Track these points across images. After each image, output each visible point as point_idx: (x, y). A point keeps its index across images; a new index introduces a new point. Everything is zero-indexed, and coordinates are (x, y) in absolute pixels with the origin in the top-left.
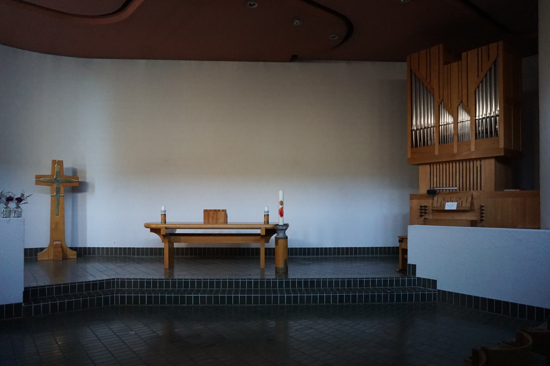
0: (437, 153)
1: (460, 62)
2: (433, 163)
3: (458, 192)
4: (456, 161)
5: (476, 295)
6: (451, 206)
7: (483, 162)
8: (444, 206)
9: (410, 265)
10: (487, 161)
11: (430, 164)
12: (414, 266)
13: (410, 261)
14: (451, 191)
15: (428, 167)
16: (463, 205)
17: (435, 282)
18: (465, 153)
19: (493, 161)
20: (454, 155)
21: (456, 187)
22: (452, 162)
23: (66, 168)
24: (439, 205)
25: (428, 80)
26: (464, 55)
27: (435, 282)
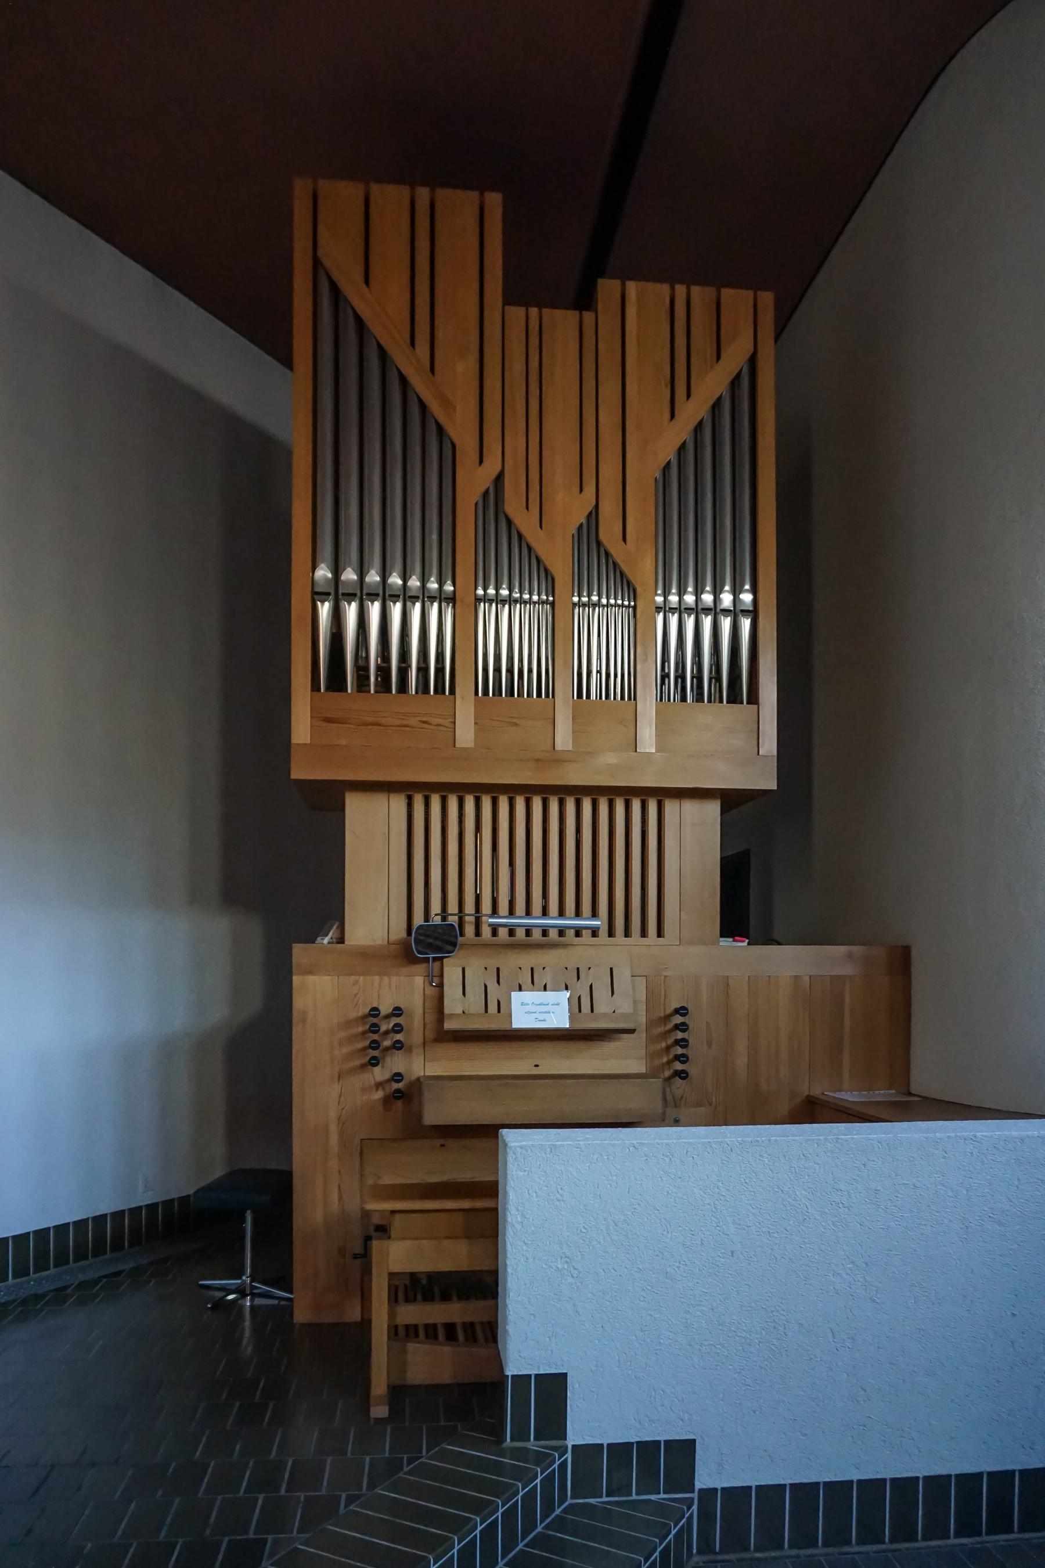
0: (466, 734)
1: (588, 317)
2: (428, 788)
3: (554, 946)
4: (563, 791)
5: (932, 1474)
6: (540, 1008)
7: (671, 807)
8: (503, 1008)
9: (522, 1380)
10: (690, 807)
11: (407, 789)
12: (553, 1388)
13: (523, 1354)
14: (520, 933)
15: (398, 804)
16: (601, 1008)
17: (683, 1451)
18: (610, 759)
19: (713, 809)
20: (556, 759)
21: (594, 914)
22: (545, 791)
23: (572, 1018)
24: (474, 1001)
25: (423, 351)
26: (607, 288)
27: (683, 1451)
